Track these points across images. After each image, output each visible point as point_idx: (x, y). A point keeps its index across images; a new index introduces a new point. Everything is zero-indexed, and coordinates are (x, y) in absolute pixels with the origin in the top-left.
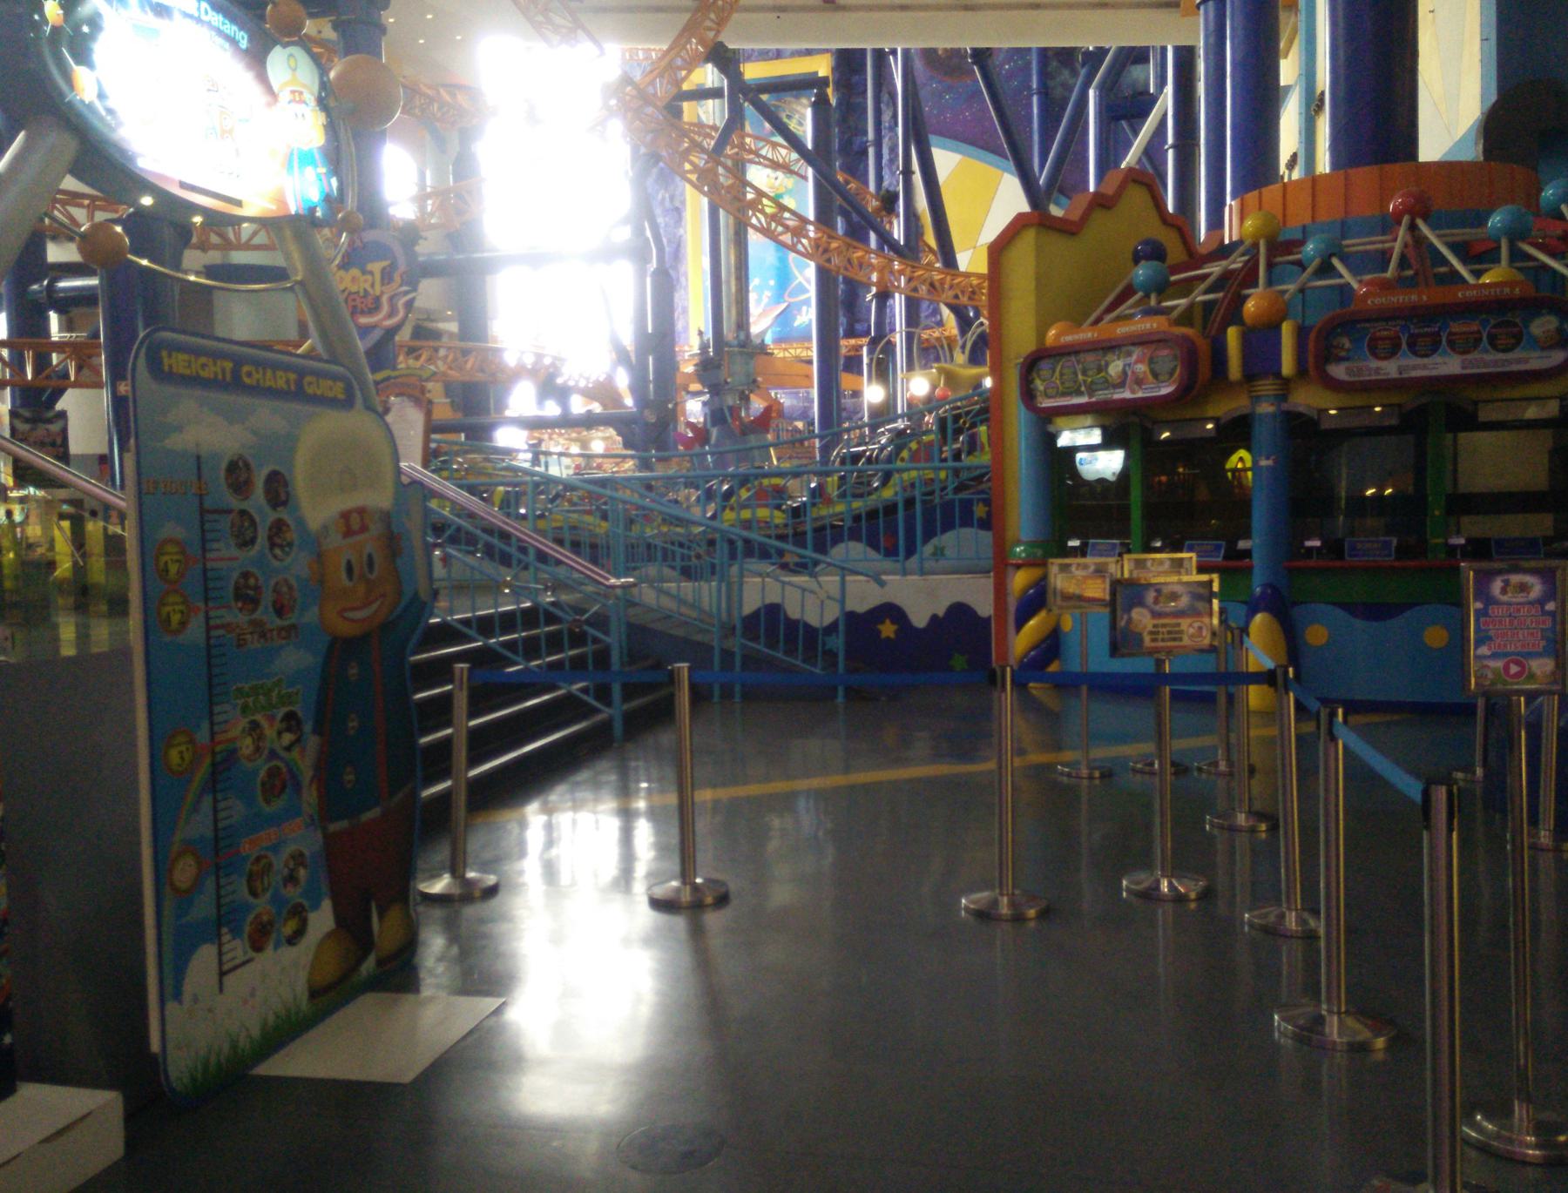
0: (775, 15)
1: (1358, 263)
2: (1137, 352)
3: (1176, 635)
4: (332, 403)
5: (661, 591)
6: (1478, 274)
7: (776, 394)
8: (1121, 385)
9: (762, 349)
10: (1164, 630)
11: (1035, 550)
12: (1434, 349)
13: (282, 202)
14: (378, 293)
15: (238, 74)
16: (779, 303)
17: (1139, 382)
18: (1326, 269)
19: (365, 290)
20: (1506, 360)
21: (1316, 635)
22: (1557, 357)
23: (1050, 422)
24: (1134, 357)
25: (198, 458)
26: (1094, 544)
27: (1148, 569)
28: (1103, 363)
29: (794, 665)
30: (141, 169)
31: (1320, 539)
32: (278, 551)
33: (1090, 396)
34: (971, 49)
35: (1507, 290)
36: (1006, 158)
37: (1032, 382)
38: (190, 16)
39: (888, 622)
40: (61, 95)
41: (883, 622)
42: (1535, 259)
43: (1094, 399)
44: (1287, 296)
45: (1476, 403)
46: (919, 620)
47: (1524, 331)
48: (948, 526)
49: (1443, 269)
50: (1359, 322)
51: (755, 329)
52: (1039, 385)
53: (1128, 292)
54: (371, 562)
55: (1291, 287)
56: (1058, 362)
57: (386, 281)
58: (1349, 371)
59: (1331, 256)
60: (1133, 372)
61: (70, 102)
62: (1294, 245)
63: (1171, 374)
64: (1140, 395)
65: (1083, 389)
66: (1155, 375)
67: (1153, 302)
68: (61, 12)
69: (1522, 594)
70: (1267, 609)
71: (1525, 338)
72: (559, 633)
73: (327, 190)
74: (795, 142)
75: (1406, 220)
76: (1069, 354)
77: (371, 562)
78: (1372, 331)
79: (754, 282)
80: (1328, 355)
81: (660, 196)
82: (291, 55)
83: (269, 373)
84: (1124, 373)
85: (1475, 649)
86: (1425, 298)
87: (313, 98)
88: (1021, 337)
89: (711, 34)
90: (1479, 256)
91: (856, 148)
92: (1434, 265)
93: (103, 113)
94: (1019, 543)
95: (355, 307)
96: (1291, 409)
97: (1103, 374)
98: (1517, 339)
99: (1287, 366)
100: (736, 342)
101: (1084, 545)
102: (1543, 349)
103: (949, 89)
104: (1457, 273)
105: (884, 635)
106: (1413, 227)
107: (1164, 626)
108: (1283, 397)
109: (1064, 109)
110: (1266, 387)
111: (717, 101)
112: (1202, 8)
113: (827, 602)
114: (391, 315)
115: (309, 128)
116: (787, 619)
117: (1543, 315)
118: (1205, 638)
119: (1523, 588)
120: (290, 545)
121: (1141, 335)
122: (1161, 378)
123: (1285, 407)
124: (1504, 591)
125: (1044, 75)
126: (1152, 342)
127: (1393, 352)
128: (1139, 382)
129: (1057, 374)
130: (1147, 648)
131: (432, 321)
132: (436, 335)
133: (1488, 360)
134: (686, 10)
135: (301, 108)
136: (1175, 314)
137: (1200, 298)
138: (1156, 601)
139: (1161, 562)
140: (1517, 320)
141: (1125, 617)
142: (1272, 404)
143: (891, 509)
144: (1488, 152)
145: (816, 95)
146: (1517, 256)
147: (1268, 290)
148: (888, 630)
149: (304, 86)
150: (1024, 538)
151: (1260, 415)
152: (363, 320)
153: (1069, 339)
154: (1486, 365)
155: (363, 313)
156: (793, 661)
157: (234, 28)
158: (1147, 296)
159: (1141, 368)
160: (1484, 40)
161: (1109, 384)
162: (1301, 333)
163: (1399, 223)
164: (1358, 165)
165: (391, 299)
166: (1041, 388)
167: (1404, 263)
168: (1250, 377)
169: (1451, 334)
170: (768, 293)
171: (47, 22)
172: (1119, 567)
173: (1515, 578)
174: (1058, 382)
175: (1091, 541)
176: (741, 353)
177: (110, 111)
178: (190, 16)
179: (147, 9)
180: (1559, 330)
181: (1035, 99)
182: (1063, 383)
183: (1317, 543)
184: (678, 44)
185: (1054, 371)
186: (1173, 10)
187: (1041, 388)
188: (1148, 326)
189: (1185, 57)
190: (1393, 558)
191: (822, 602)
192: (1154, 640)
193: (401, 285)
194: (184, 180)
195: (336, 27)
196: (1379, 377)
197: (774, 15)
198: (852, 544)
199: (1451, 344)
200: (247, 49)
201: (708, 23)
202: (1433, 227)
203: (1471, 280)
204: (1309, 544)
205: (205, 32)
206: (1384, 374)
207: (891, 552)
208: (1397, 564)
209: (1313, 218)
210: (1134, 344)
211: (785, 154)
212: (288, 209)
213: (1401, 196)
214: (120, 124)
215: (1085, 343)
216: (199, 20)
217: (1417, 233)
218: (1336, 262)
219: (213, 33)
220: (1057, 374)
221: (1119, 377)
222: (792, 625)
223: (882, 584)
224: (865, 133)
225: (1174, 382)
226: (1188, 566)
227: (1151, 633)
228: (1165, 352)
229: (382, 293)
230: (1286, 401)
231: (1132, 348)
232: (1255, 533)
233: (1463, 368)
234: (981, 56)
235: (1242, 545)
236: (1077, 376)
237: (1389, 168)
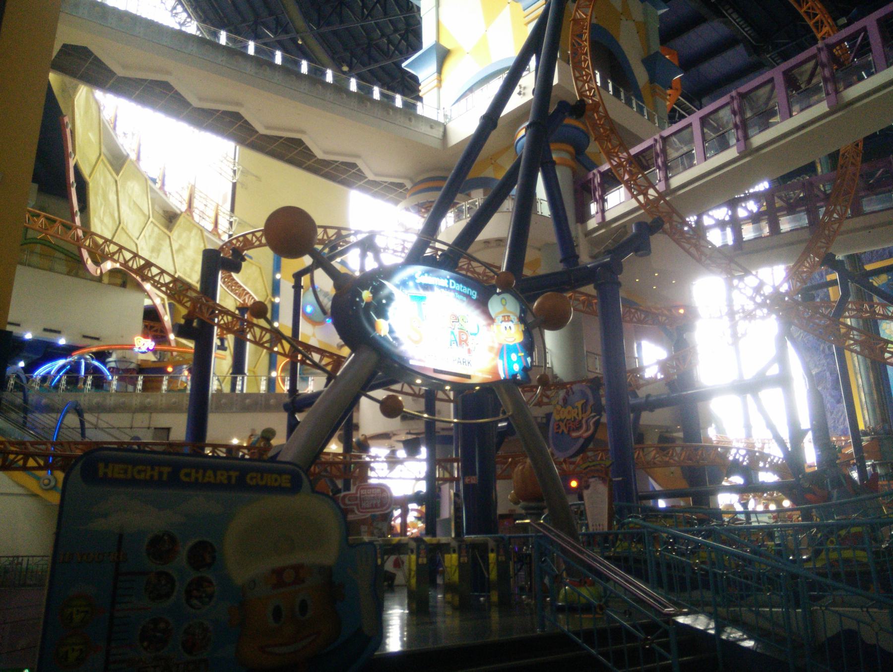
4: (279, 490)
5: (758, 614)
19: (574, 418)
25: (121, 536)
30: (412, 365)
32: (195, 602)
38: (444, 288)
40: (368, 333)
54: (304, 606)
61: (373, 337)
68: (371, 295)
77: (304, 606)
81: (821, 348)
83: (210, 473)
85: (61, 222)
87: (516, 318)
93: (391, 340)
95: (569, 428)
111: (835, 287)
114: (587, 430)
115: (513, 334)
120: (211, 597)
132: (673, 440)
149: (511, 312)
152: (574, 434)
155: (574, 430)
157: (469, 289)
165: (587, 421)
171: (363, 301)
177: (395, 339)
178: (444, 288)
179: (420, 288)
193: (591, 413)
194: (436, 368)
205: (452, 294)
212: (498, 374)
214: (400, 344)
216: (448, 289)
219: (457, 294)
229: (582, 418)
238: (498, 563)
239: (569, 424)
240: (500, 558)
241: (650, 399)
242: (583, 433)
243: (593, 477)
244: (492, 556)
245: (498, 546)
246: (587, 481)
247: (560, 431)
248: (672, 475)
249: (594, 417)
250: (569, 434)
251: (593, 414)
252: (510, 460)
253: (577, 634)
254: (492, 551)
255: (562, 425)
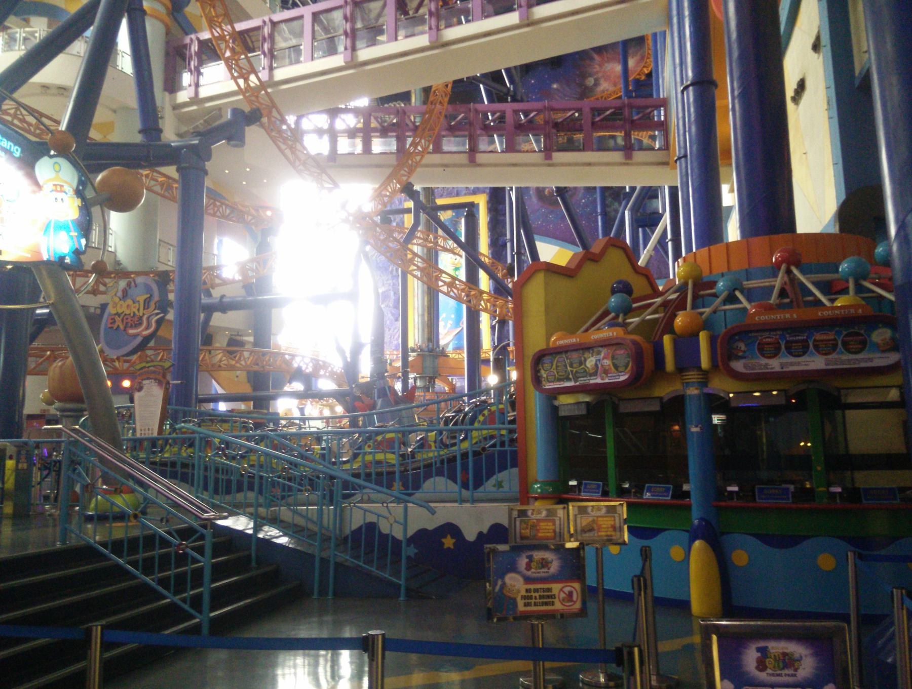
0: (442, 169)
1: (750, 295)
2: (604, 351)
3: (549, 598)
5: (295, 512)
6: (832, 301)
7: (452, 379)
8: (595, 374)
9: (443, 354)
10: (537, 594)
11: (548, 488)
12: (804, 351)
13: (39, 253)
14: (141, 314)
15: (14, 175)
16: (456, 327)
17: (606, 372)
18: (731, 299)
20: (857, 359)
21: (740, 558)
22: (893, 358)
23: (555, 398)
24: (602, 355)
26: (586, 484)
27: (588, 514)
28: (583, 359)
29: (371, 571)
31: (738, 486)
33: (576, 381)
34: (556, 187)
35: (852, 311)
36: (578, 246)
37: (538, 371)
39: (449, 536)
41: (445, 537)
42: (873, 292)
43: (578, 384)
44: (704, 316)
45: (839, 389)
46: (470, 535)
47: (868, 339)
48: (502, 468)
49: (811, 298)
50: (751, 332)
51: (442, 342)
52: (544, 374)
53: (606, 313)
55: (707, 310)
56: (555, 358)
57: (146, 307)
58: (745, 366)
59: (735, 289)
60: (602, 365)
62: (712, 284)
63: (626, 367)
64: (607, 381)
65: (571, 376)
66: (616, 367)
67: (620, 320)
69: (786, 671)
70: (702, 538)
71: (868, 346)
72: (168, 555)
73: (76, 246)
74: (456, 240)
75: (784, 267)
76: (560, 353)
78: (760, 338)
79: (442, 316)
80: (731, 355)
81: (390, 269)
82: (56, 163)
84: (596, 365)
86: (795, 316)
88: (536, 340)
89: (405, 178)
90: (831, 289)
91: (500, 242)
92: (804, 296)
94: (536, 482)
96: (711, 392)
97: (583, 366)
98: (863, 345)
99: (705, 363)
100: (426, 349)
101: (579, 484)
102: (883, 352)
103: (551, 212)
104: (820, 301)
105: (446, 546)
106: (789, 272)
107: (536, 590)
108: (704, 383)
109: (615, 221)
110: (692, 376)
112: (678, 162)
113: (395, 525)
114: (147, 328)
115: (70, 208)
116: (380, 532)
117: (880, 328)
118: (575, 602)
119: (788, 661)
121: (605, 340)
122: (620, 369)
123: (706, 390)
124: (761, 666)
125: (604, 205)
126: (613, 345)
127: (775, 354)
128: (606, 372)
129: (554, 366)
130: (520, 612)
131: (240, 336)
132: (242, 344)
133: (843, 359)
134: (389, 166)
135: (60, 196)
136: (631, 327)
137: (648, 317)
138: (528, 567)
139: (599, 509)
140: (862, 332)
141: (500, 582)
142: (697, 389)
143: (465, 455)
144: (842, 229)
145: (467, 212)
146: (860, 289)
147: (692, 311)
148: (449, 542)
150: (540, 479)
151: (689, 395)
152: (131, 331)
153: (561, 342)
154: (843, 363)
155: (131, 327)
156: (370, 568)
157: (10, 143)
158: (617, 317)
159: (607, 362)
160: (835, 164)
161: (586, 373)
162: (712, 340)
163: (779, 269)
164: (757, 235)
165: (148, 318)
166: (545, 376)
167: (783, 293)
168: (681, 369)
169: (815, 340)
170: (450, 322)
172: (566, 510)
173: (777, 647)
174: (555, 371)
175: (584, 482)
176: (430, 355)
180: (893, 339)
181: (599, 218)
182: (558, 373)
183: (736, 489)
184: (384, 185)
185: (552, 365)
186: (665, 166)
187: (545, 376)
188: (611, 334)
189: (673, 191)
190: (791, 501)
191: (391, 525)
192: (526, 605)
193: (154, 310)
195: (178, 170)
196: (767, 371)
197: (442, 169)
198: (438, 479)
199: (816, 347)
200: (20, 157)
201: (403, 172)
202: (803, 272)
203: (828, 304)
204: (730, 489)
206: (772, 368)
207: (465, 486)
208: (794, 506)
209: (729, 268)
210: (602, 346)
211: (451, 244)
213: (779, 252)
215: (573, 345)
217: (792, 276)
218: (738, 294)
220: (554, 366)
221: (593, 369)
222: (385, 537)
223: (433, 512)
224: (505, 235)
225: (627, 373)
226: (621, 512)
227: (524, 597)
228: (622, 352)
229: (144, 314)
230: (707, 386)
231: (601, 349)
232: (691, 477)
233: (827, 364)
234: (561, 191)
235: (686, 487)
236: (567, 368)
237: (775, 237)
238: (17, 470)
239: (127, 319)
240: (20, 466)
241: (225, 300)
242: (140, 332)
243: (148, 379)
244: (10, 464)
245: (19, 453)
246: (140, 383)
247: (115, 327)
248: (236, 379)
249: (157, 314)
250: (125, 330)
251: (157, 311)
252: (48, 353)
253: (104, 545)
254: (11, 458)
255: (118, 319)
